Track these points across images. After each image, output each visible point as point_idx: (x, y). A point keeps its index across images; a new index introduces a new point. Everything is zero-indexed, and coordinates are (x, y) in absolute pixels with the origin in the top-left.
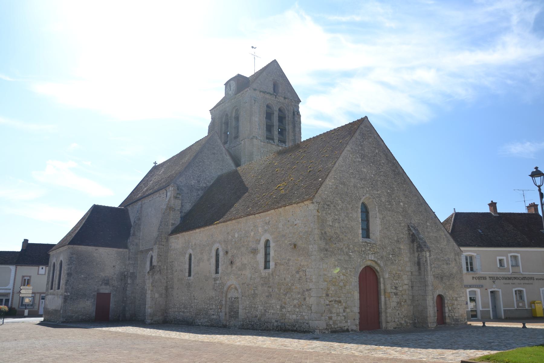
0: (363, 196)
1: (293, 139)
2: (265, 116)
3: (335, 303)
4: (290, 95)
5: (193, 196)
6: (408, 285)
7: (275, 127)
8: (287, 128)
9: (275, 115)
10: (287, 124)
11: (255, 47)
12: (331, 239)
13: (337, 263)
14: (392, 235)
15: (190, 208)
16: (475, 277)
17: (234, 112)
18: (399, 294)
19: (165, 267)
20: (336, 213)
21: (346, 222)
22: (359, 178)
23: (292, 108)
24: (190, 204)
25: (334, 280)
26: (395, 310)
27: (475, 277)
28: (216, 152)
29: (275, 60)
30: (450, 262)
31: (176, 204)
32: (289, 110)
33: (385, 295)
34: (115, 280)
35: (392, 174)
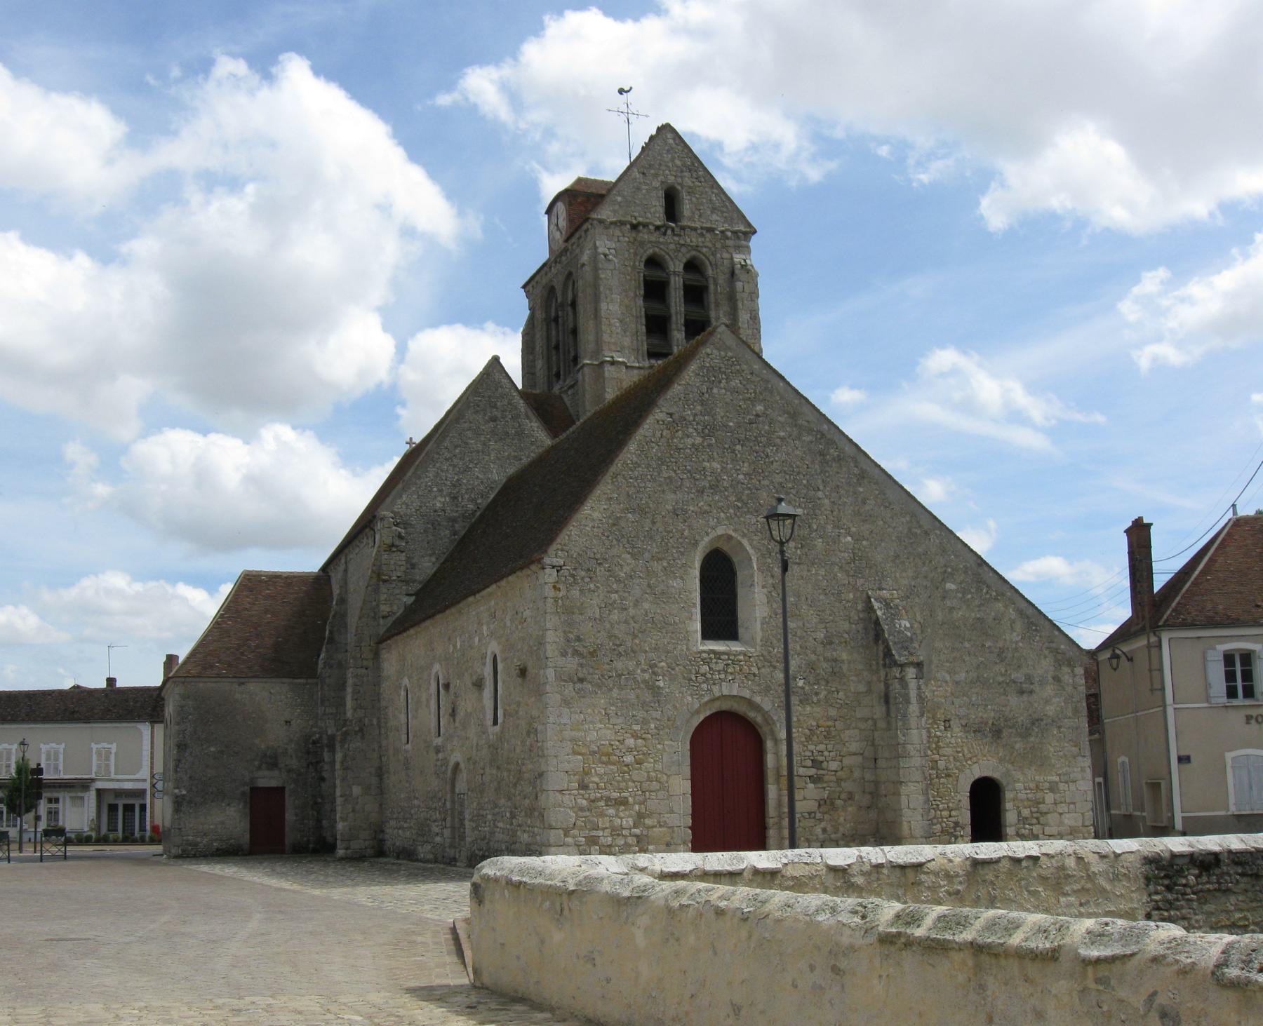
3: (607, 805)
6: (862, 754)
7: (674, 318)
11: (628, 89)
12: (595, 651)
16: (1254, 715)
18: (826, 778)
19: (375, 722)
21: (646, 606)
24: (433, 559)
26: (813, 820)
27: (1254, 715)
32: (716, 265)
34: (291, 756)
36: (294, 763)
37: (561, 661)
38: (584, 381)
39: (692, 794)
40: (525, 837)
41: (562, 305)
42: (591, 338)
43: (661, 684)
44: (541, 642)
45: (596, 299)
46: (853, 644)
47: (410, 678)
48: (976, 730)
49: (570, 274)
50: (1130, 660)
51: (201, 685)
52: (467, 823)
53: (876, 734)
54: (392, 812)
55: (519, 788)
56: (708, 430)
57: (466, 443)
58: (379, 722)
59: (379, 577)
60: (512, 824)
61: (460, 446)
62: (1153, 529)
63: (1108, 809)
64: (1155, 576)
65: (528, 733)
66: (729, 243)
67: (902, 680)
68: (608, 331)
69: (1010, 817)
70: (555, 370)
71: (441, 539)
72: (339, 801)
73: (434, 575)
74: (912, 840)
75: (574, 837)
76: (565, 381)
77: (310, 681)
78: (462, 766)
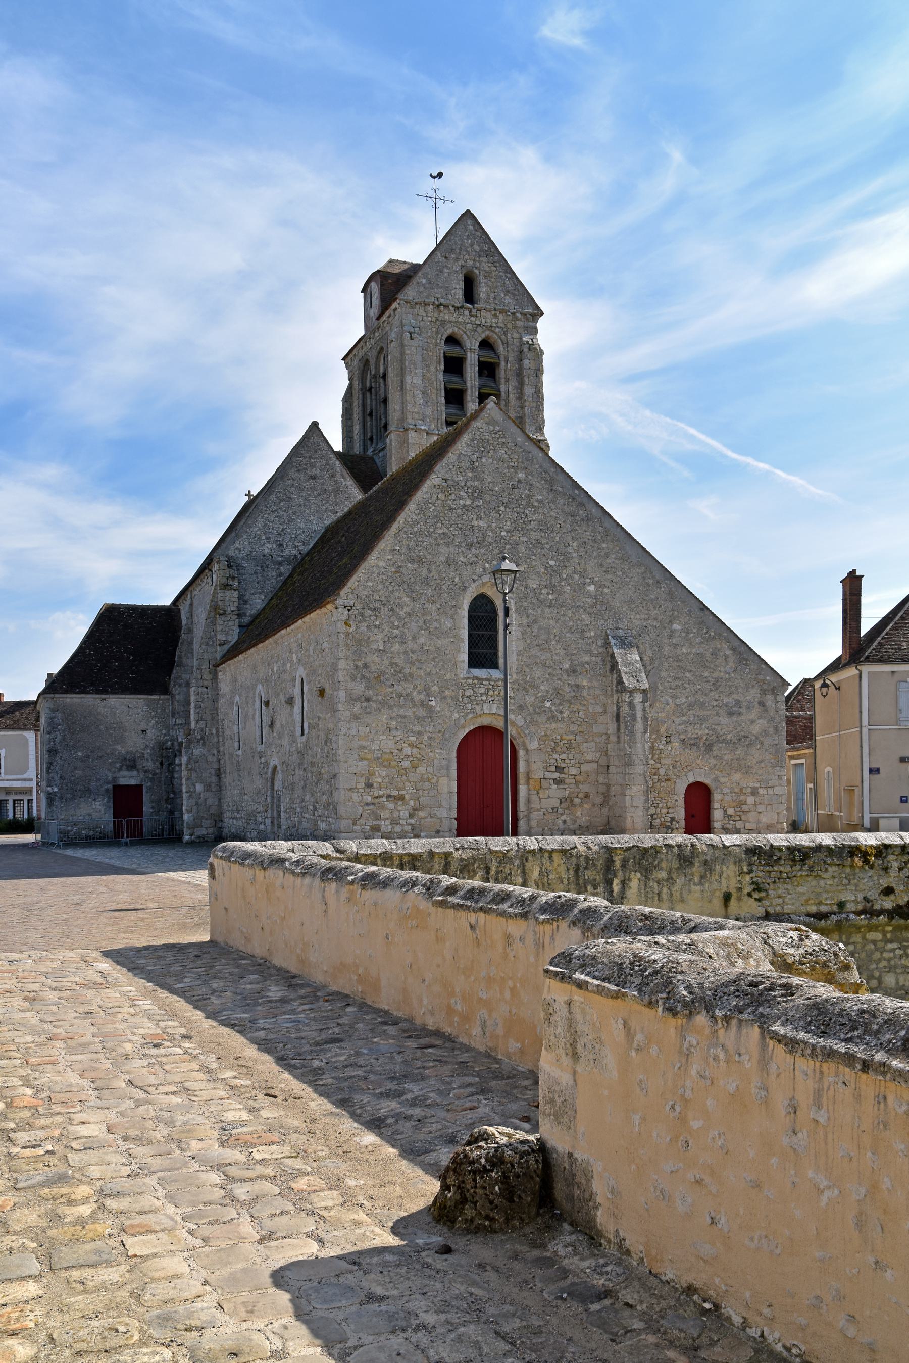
0: (474, 580)
4: (511, 301)
7: (469, 392)
9: (468, 362)
12: (379, 676)
13: (394, 723)
14: (556, 658)
18: (567, 781)
19: (214, 732)
20: (396, 623)
21: (422, 640)
22: (463, 545)
25: (386, 756)
29: (468, 212)
30: (743, 710)
32: (507, 344)
33: (528, 783)
35: (564, 522)
36: (150, 765)
37: (351, 685)
38: (391, 444)
39: (458, 793)
40: (323, 826)
41: (375, 376)
42: (398, 407)
43: (433, 703)
44: (335, 669)
45: (402, 373)
46: (592, 673)
47: (240, 695)
48: (690, 744)
49: (382, 349)
50: (838, 688)
51: (68, 700)
52: (282, 814)
53: (609, 746)
54: (229, 806)
55: (319, 786)
56: (477, 494)
57: (290, 498)
58: (217, 732)
59: (217, 611)
60: (314, 815)
61: (284, 500)
62: (864, 582)
63: (816, 809)
64: (862, 619)
65: (326, 742)
66: (519, 323)
67: (631, 705)
69: (717, 815)
70: (369, 434)
71: (269, 580)
72: (185, 796)
73: (264, 609)
74: (634, 831)
75: (361, 825)
76: (377, 444)
77: (162, 697)
78: (279, 768)
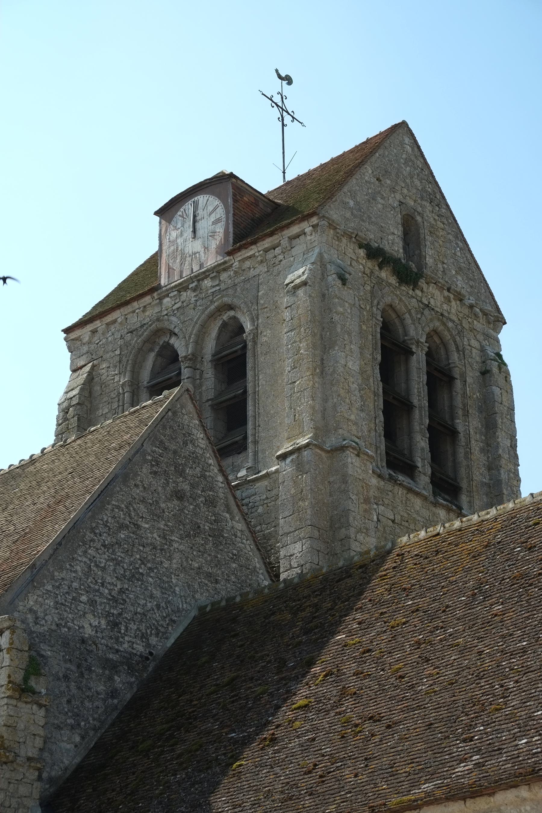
1: (486, 480)
2: (379, 358)
5: (88, 693)
8: (460, 428)
10: (460, 412)
15: (78, 760)
17: (214, 333)
23: (474, 343)
24: (77, 739)
28: (187, 487)
29: (403, 125)
31: (21, 726)
57: (138, 527)
68: (347, 401)
71: (91, 699)
